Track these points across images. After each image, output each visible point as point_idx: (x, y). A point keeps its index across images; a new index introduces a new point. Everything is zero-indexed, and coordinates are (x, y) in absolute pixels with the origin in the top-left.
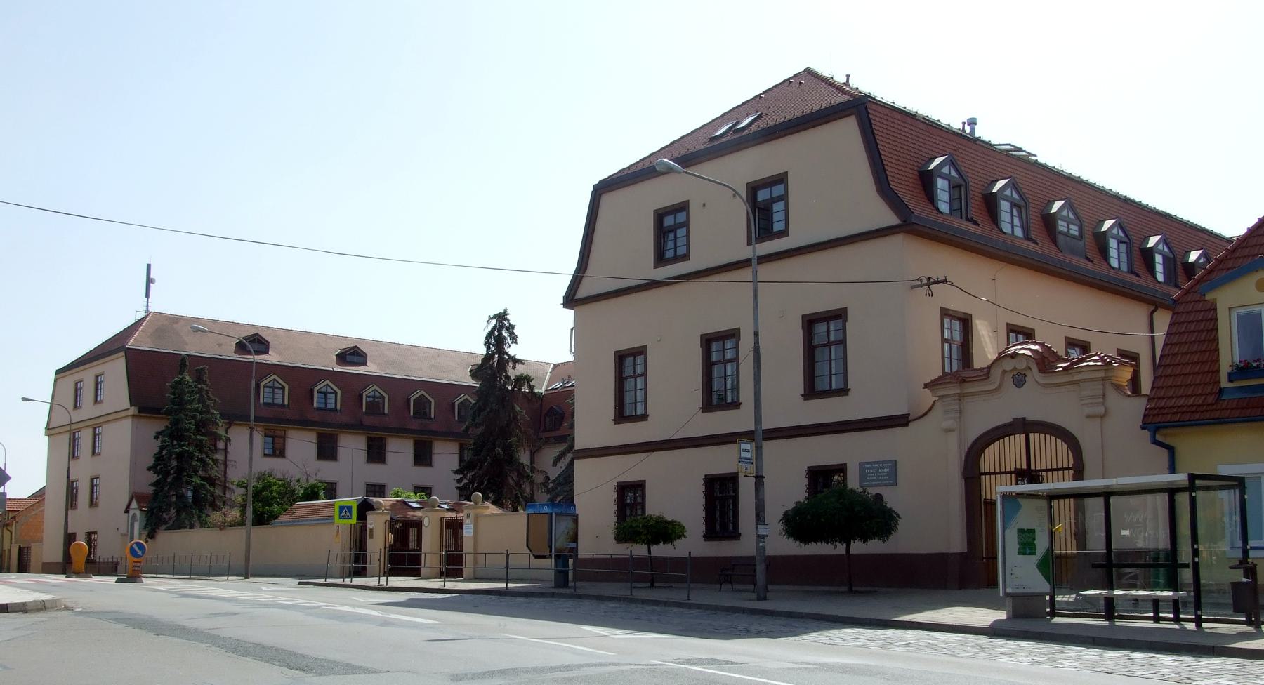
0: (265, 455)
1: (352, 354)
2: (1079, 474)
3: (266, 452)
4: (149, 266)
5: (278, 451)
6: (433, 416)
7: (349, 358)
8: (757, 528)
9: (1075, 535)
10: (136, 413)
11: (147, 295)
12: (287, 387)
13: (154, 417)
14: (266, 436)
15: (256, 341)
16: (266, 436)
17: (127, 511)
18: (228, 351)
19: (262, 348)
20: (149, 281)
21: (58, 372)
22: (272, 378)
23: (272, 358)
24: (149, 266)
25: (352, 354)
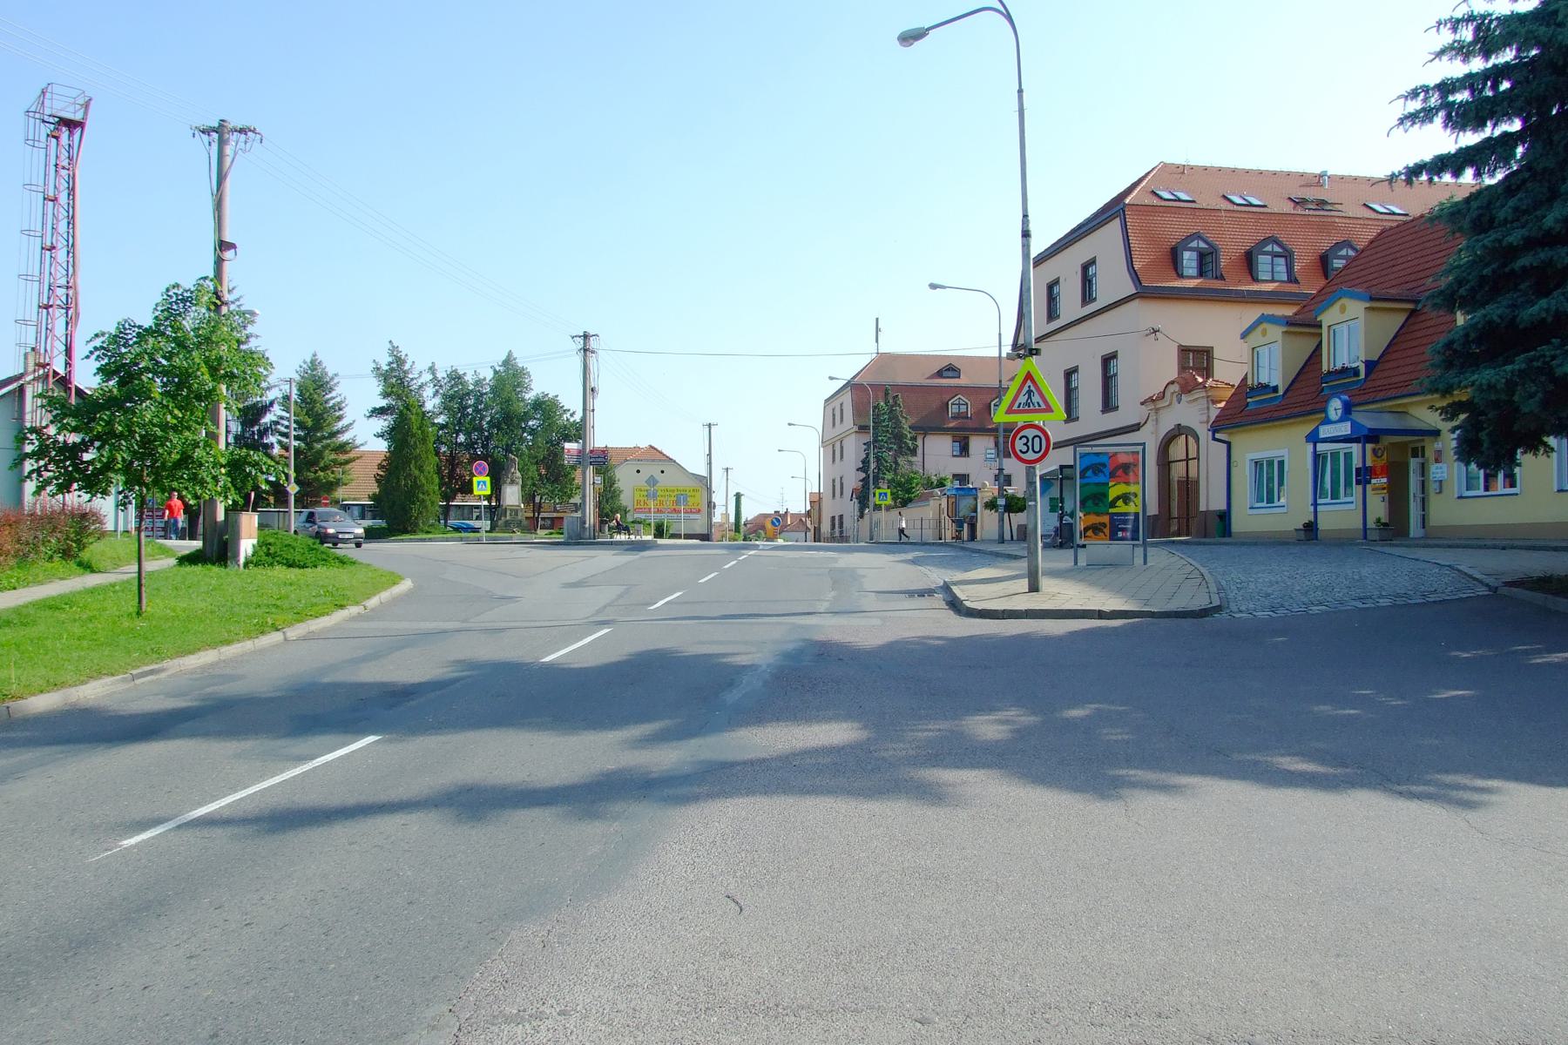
0: (954, 456)
1: (948, 370)
2: (1212, 253)
3: (955, 453)
4: (877, 319)
5: (964, 450)
6: (969, 416)
7: (945, 374)
8: (1315, 504)
9: (1487, 233)
10: (857, 430)
11: (877, 341)
12: (969, 403)
13: (1269, 427)
14: (954, 441)
15: (950, 369)
16: (954, 441)
17: (851, 500)
18: (918, 378)
19: (955, 374)
20: (878, 330)
21: (826, 401)
22: (958, 397)
23: (963, 381)
24: (877, 319)
25: (948, 370)
